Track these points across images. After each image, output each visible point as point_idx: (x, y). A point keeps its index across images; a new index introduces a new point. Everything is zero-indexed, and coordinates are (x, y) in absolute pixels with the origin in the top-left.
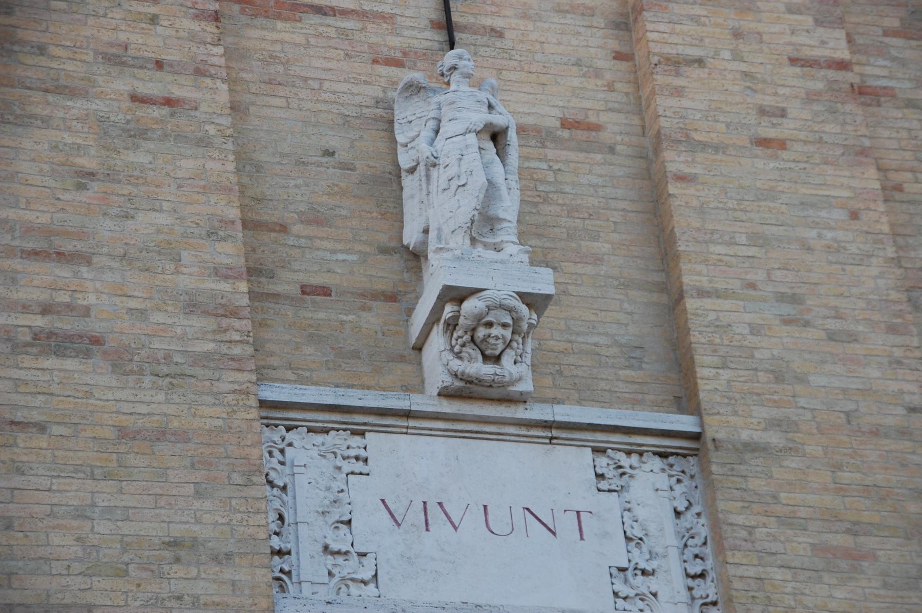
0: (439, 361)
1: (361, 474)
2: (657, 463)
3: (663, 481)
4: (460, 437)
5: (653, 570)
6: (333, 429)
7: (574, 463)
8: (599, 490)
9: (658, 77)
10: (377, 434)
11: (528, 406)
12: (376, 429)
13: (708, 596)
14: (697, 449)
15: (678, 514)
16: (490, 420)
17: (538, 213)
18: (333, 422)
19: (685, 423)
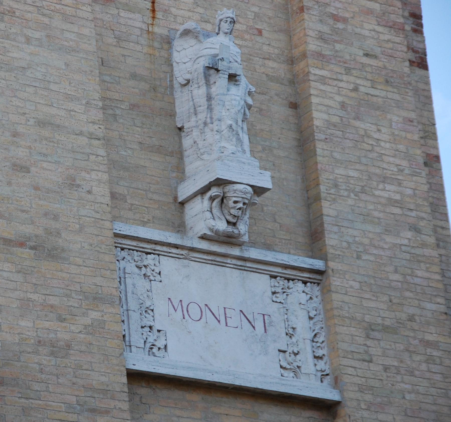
0: (202, 218)
1: (276, 302)
2: (300, 285)
3: (304, 298)
4: (215, 265)
5: (298, 352)
6: (309, 282)
7: (261, 283)
8: (273, 301)
9: (139, 24)
10: (260, 274)
11: (243, 248)
12: (251, 269)
13: (325, 370)
14: (321, 280)
15: (311, 318)
16: (202, 251)
17: (382, 161)
18: (132, 246)
19: (318, 264)
